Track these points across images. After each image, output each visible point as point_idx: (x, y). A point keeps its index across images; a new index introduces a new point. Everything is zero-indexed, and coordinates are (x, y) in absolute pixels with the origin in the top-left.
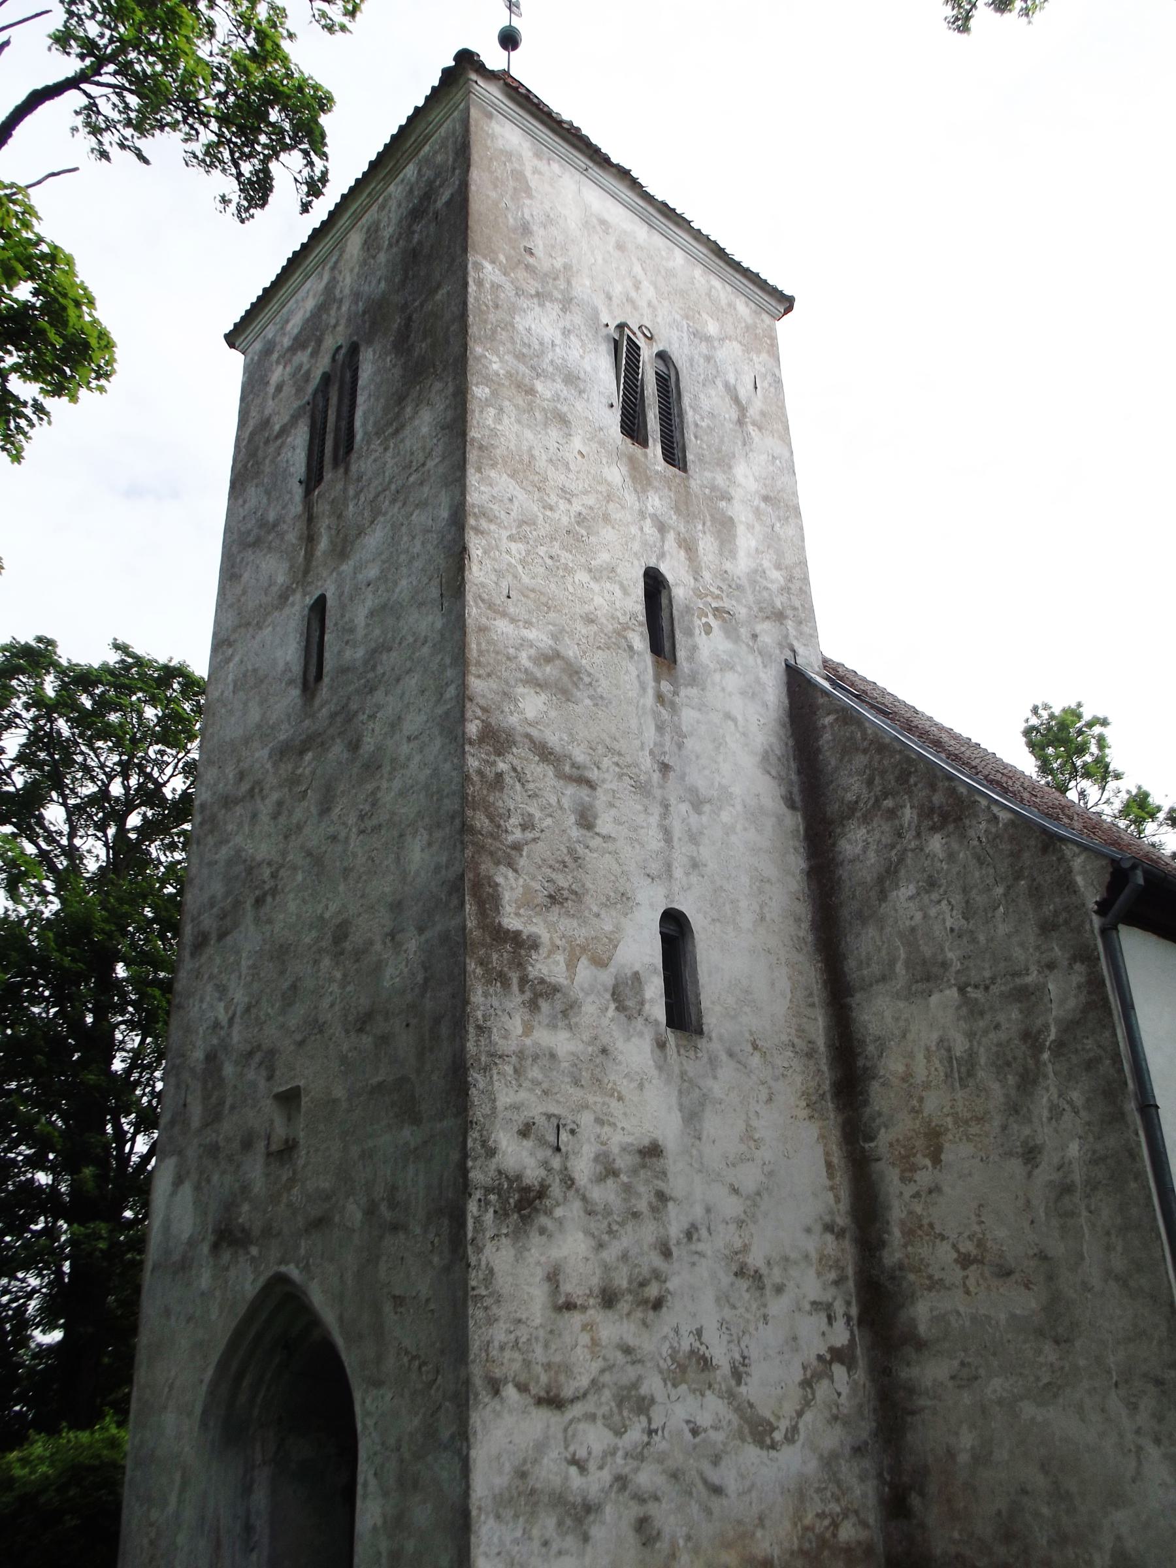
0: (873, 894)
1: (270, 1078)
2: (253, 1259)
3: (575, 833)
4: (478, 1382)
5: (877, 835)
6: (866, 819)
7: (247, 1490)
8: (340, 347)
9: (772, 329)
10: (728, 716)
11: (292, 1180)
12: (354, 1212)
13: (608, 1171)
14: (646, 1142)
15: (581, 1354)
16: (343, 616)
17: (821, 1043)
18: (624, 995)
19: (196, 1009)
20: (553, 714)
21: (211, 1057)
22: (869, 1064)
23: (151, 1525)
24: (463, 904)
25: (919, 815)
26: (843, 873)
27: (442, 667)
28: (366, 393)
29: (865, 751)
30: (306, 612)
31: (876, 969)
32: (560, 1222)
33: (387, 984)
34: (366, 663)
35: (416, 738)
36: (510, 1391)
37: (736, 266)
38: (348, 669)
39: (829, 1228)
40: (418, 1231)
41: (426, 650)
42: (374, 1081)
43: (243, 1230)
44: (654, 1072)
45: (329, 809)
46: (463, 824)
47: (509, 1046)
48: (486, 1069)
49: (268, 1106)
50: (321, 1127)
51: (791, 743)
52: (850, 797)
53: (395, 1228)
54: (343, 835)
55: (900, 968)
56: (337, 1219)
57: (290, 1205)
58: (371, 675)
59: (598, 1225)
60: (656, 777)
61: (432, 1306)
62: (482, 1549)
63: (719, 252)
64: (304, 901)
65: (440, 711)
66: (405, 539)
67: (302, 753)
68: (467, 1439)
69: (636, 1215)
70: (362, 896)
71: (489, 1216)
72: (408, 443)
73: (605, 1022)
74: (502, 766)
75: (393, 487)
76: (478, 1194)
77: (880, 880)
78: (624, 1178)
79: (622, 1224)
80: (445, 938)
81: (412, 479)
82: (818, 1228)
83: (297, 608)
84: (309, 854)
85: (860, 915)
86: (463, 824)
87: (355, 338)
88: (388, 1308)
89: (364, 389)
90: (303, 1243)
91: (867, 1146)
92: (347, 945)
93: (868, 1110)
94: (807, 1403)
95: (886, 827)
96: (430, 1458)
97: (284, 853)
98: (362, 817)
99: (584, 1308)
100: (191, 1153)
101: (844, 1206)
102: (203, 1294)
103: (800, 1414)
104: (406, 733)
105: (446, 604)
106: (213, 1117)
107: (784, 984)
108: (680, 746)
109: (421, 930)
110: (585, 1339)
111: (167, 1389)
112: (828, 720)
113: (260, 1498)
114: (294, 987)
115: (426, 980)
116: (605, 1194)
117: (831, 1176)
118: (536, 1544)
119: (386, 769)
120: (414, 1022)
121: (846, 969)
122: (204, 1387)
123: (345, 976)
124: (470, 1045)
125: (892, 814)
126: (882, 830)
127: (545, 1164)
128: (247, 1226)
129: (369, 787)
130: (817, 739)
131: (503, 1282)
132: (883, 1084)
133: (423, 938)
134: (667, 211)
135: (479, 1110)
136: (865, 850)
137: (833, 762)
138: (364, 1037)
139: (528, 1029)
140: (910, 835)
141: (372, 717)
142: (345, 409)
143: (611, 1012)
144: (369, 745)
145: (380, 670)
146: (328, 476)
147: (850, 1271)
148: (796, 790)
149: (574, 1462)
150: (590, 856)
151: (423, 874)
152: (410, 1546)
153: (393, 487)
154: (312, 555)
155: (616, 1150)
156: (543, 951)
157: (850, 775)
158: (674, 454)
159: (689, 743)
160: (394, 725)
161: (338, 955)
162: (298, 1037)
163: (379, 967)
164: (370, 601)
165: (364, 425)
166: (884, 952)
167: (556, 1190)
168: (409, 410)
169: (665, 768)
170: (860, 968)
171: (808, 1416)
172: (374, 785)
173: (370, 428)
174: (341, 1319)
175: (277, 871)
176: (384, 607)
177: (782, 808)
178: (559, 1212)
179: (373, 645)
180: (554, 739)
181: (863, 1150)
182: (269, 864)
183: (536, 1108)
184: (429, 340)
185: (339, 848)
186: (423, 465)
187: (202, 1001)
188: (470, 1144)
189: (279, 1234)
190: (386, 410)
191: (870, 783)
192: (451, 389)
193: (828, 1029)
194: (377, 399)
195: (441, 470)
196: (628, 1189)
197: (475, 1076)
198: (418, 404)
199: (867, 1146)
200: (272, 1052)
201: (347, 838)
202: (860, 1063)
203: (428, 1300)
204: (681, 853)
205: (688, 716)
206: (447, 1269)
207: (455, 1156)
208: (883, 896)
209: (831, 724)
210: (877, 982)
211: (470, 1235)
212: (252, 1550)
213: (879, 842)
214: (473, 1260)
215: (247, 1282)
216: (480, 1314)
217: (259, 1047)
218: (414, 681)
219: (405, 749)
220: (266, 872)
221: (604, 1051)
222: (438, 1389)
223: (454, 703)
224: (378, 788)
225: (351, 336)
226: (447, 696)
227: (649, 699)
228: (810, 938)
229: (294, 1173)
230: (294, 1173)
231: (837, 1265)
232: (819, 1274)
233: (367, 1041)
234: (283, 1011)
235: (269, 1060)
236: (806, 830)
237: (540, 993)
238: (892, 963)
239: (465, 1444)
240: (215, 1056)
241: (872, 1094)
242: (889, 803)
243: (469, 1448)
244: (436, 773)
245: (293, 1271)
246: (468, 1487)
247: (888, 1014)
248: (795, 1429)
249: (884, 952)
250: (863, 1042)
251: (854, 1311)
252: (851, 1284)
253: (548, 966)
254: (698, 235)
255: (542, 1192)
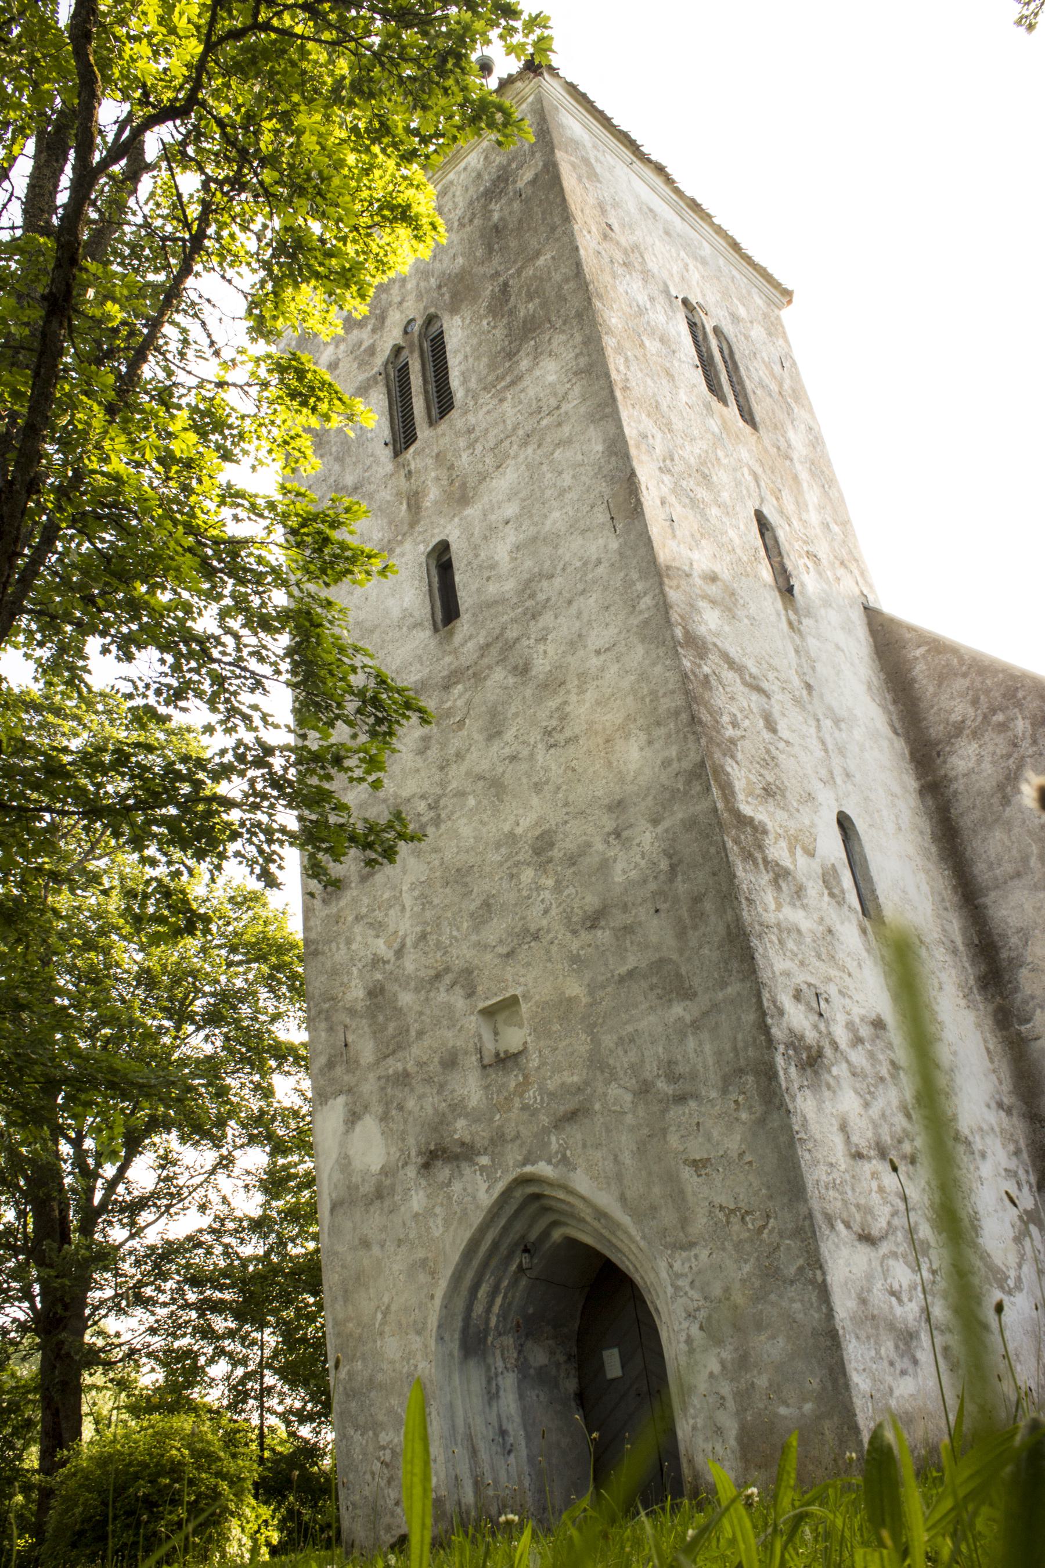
0: (995, 801)
1: (470, 994)
2: (483, 1168)
3: (767, 735)
4: (819, 1217)
5: (991, 748)
6: (975, 734)
7: (492, 1396)
8: (411, 321)
9: (778, 318)
10: (838, 647)
11: (526, 1083)
12: (619, 1094)
13: (857, 1041)
14: (873, 1016)
15: (876, 1198)
16: (477, 556)
17: (959, 940)
18: (829, 879)
19: (343, 951)
20: (727, 628)
21: (375, 992)
22: (1013, 954)
23: (384, 1448)
24: (708, 789)
25: (1033, 724)
26: (959, 785)
27: (628, 584)
28: (460, 357)
29: (965, 675)
30: (423, 559)
31: (1009, 868)
32: (836, 1078)
33: (619, 878)
34: (520, 593)
35: (608, 650)
36: (840, 1227)
37: (748, 259)
38: (496, 602)
39: (1000, 1105)
40: (713, 1094)
41: (601, 570)
42: (623, 970)
43: (463, 1144)
44: (865, 954)
45: (499, 733)
46: (693, 717)
47: (770, 918)
48: (760, 936)
49: (473, 1022)
50: (556, 1027)
51: (882, 676)
52: (956, 717)
53: (681, 1099)
54: (525, 752)
55: (1034, 862)
56: (597, 1106)
57: (525, 1108)
58: (530, 603)
59: (862, 1086)
60: (805, 692)
61: (748, 1158)
62: (853, 1364)
63: (735, 246)
64: (482, 822)
65: (635, 621)
66: (549, 475)
67: (446, 688)
68: (821, 1267)
69: (882, 1079)
70: (566, 804)
71: (793, 1070)
72: (531, 393)
73: (825, 906)
74: (706, 669)
75: (521, 432)
76: (781, 1048)
77: (1001, 787)
78: (868, 1046)
79: (876, 1086)
80: (690, 824)
81: (544, 422)
82: (993, 1105)
83: (409, 557)
84: (480, 777)
85: (983, 821)
86: (693, 717)
87: (432, 310)
88: (687, 1173)
89: (457, 352)
90: (553, 1139)
91: (1023, 1028)
92: (556, 853)
93: (1019, 996)
94: (1022, 1257)
95: (1000, 739)
96: (773, 1297)
97: (443, 784)
98: (548, 733)
99: (869, 1159)
100: (369, 1087)
101: (1007, 1086)
102: (417, 1215)
103: (1020, 1266)
104: (592, 647)
105: (619, 527)
106: (392, 1046)
107: (925, 888)
108: (813, 668)
109: (655, 822)
110: (874, 1185)
111: (379, 1316)
112: (919, 652)
113: (509, 1403)
114: (487, 905)
115: (673, 867)
116: (858, 1057)
117: (992, 1061)
118: (886, 1364)
119: (573, 683)
120: (663, 907)
121: (976, 872)
122: (438, 1302)
123: (558, 882)
124: (745, 913)
125: (1003, 727)
126: (995, 743)
127: (816, 1027)
128: (468, 1139)
129: (552, 704)
130: (910, 670)
131: (814, 1128)
132: (1033, 970)
133: (660, 829)
134: (694, 206)
135: (765, 975)
136: (979, 762)
137: (931, 689)
138: (599, 933)
139: (779, 907)
140: (1026, 744)
141: (543, 639)
142: (431, 374)
143: (826, 898)
144: (541, 666)
145: (541, 597)
146: (423, 432)
147: (1022, 1144)
148: (894, 717)
149: (893, 1293)
150: (782, 757)
151: (647, 771)
152: (762, 1381)
153: (521, 432)
154: (419, 507)
155: (857, 1020)
156: (772, 836)
157: (952, 698)
158: (748, 416)
159: (819, 666)
160: (575, 643)
161: (542, 867)
162: (503, 950)
163: (604, 866)
164: (511, 537)
165: (465, 381)
166: (1014, 852)
167: (828, 1051)
168: (525, 364)
169: (809, 687)
170: (991, 867)
171: (1025, 1268)
172: (559, 701)
173: (473, 384)
174: (623, 1198)
175: (437, 802)
176: (534, 539)
177: (891, 735)
178: (835, 1071)
179: (526, 576)
180: (733, 652)
181: (1019, 1033)
182: (423, 797)
183: (800, 978)
184: (537, 301)
185: (524, 766)
186: (558, 408)
187: (349, 942)
188: (766, 1004)
189: (518, 1136)
190: (492, 366)
191: (975, 702)
192: (578, 338)
193: (964, 930)
194: (478, 358)
195: (582, 410)
196: (871, 1055)
197: (755, 942)
198: (536, 356)
199: (1023, 1028)
200: (468, 972)
201: (532, 756)
202: (1004, 954)
203: (741, 1155)
204: (836, 761)
205: (812, 643)
206: (762, 1121)
207: (750, 1017)
208: (1006, 801)
209: (924, 656)
210: (1012, 878)
211: (784, 1085)
212: (510, 1452)
213: (994, 753)
214: (791, 1107)
215: (479, 1190)
216: (807, 1156)
217: (447, 970)
218: (592, 600)
219: (595, 662)
220: (421, 806)
221: (830, 931)
222: (771, 1232)
223: (653, 611)
224: (565, 703)
225: (426, 308)
226: (642, 606)
227: (784, 625)
228: (934, 849)
229: (526, 1077)
230: (526, 1077)
231: (1012, 1139)
232: (1004, 1146)
233: (603, 936)
234: (477, 928)
235: (467, 980)
236: (912, 754)
237: (780, 875)
238: (1025, 859)
239: (818, 1272)
240: (382, 990)
241: (1022, 981)
242: (1000, 717)
243: (824, 1274)
244: (643, 677)
245: (544, 1169)
246: (831, 1309)
247: (1028, 907)
248: (1019, 1279)
249: (1014, 852)
250: (1004, 936)
251: (1033, 1179)
252: (1025, 1155)
253: (778, 851)
254: (719, 230)
255: (820, 1054)
